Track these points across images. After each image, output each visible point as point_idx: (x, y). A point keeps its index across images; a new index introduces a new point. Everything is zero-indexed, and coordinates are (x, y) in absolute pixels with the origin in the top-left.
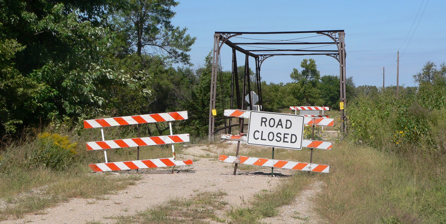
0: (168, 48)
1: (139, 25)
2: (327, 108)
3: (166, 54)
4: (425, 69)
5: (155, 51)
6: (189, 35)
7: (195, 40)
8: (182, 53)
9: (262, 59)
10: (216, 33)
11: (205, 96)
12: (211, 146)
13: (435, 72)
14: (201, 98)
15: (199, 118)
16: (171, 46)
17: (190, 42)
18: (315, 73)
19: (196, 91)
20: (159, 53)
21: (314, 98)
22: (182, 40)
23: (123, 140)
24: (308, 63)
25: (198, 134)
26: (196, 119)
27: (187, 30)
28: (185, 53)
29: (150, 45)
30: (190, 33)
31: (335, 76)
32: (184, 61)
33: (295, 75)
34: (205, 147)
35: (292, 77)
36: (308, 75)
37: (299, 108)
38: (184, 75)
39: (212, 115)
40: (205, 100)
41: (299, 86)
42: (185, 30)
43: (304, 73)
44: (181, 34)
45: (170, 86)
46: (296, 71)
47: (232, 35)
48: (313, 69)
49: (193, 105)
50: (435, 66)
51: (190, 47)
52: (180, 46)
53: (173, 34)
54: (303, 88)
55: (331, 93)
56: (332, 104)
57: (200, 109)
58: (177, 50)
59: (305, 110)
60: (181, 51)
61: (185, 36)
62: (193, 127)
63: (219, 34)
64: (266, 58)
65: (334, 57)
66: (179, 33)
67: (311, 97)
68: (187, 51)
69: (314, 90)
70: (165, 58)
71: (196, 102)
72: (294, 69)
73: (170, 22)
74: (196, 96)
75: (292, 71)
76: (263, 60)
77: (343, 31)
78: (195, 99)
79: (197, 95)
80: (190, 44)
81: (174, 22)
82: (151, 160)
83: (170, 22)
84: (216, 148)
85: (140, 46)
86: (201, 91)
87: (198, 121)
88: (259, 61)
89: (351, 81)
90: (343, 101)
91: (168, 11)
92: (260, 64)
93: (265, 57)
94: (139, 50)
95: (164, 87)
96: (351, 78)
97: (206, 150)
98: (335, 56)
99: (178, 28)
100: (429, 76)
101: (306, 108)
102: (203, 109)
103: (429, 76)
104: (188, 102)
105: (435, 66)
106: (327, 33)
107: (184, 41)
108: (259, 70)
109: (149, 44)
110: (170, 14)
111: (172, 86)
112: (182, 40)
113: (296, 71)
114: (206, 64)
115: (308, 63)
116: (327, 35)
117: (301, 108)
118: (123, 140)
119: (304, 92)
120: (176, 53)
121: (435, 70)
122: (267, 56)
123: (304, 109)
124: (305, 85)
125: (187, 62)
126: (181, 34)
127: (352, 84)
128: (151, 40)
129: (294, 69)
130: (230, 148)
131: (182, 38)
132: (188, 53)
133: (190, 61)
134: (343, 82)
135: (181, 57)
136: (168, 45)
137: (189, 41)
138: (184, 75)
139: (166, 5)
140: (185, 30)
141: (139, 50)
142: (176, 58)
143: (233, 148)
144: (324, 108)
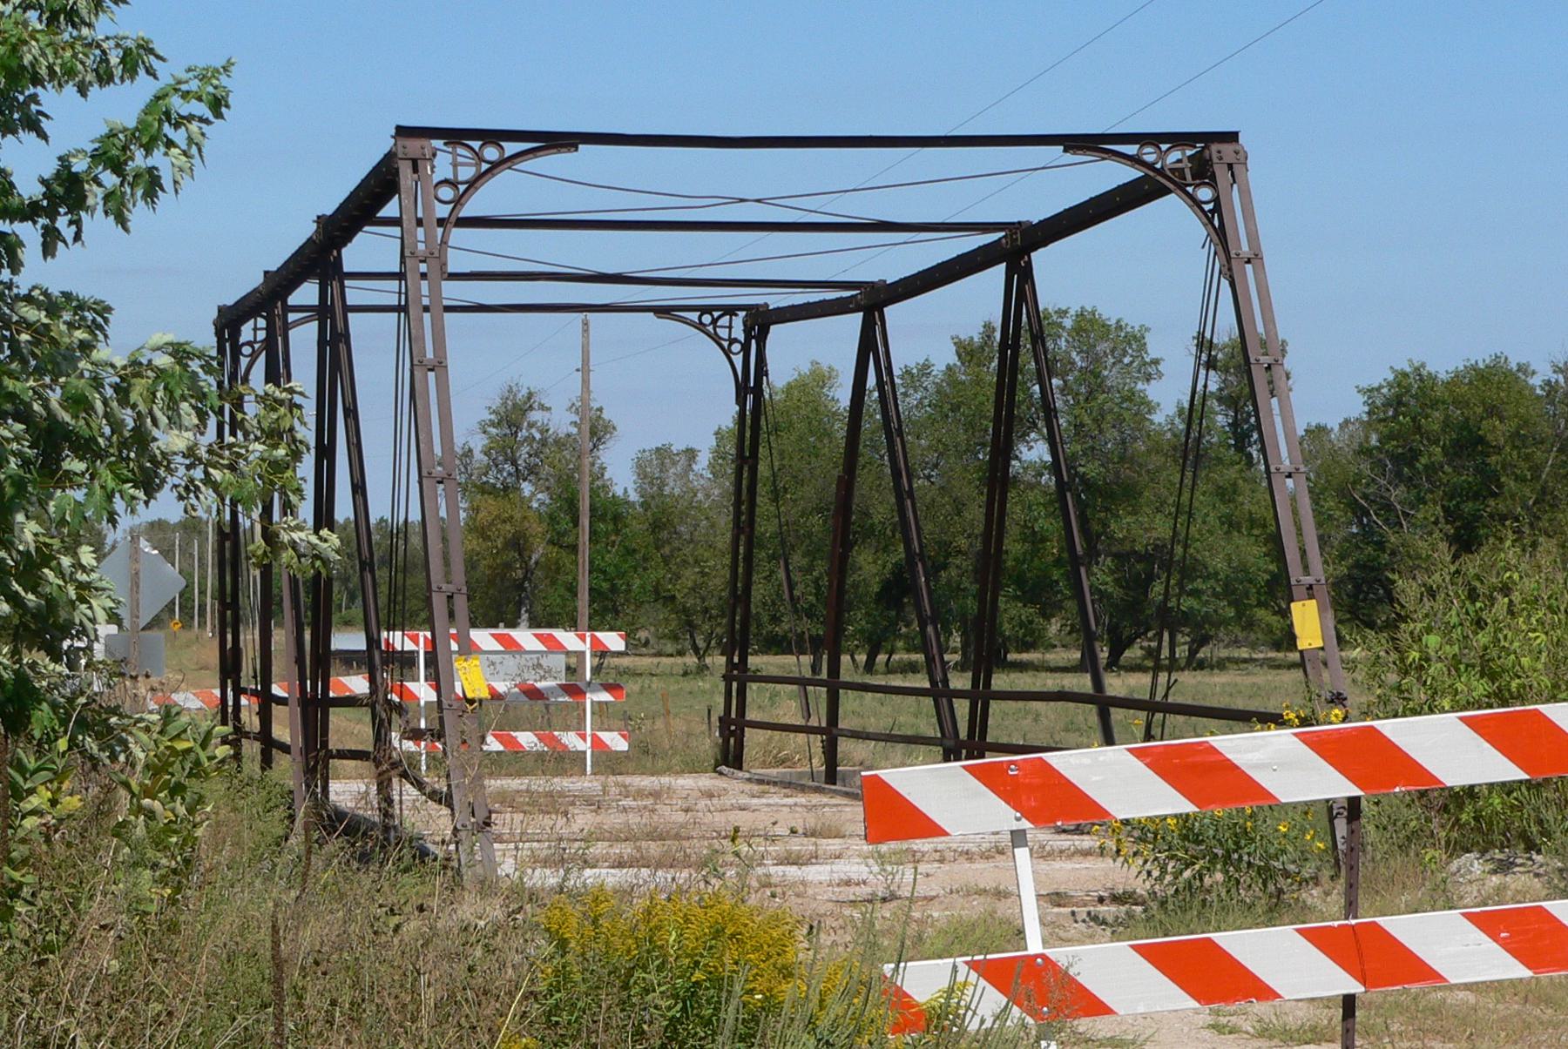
2: (613, 641)
4: (492, 424)
10: (402, 132)
13: (543, 442)
23: (1188, 807)
47: (511, 148)
50: (542, 407)
59: (479, 651)
65: (700, 326)
77: (1232, 137)
82: (1380, 920)
90: (1310, 592)
98: (707, 319)
100: (514, 463)
103: (514, 463)
105: (542, 407)
106: (1131, 149)
118: (1188, 807)
121: (544, 431)
144: (596, 642)
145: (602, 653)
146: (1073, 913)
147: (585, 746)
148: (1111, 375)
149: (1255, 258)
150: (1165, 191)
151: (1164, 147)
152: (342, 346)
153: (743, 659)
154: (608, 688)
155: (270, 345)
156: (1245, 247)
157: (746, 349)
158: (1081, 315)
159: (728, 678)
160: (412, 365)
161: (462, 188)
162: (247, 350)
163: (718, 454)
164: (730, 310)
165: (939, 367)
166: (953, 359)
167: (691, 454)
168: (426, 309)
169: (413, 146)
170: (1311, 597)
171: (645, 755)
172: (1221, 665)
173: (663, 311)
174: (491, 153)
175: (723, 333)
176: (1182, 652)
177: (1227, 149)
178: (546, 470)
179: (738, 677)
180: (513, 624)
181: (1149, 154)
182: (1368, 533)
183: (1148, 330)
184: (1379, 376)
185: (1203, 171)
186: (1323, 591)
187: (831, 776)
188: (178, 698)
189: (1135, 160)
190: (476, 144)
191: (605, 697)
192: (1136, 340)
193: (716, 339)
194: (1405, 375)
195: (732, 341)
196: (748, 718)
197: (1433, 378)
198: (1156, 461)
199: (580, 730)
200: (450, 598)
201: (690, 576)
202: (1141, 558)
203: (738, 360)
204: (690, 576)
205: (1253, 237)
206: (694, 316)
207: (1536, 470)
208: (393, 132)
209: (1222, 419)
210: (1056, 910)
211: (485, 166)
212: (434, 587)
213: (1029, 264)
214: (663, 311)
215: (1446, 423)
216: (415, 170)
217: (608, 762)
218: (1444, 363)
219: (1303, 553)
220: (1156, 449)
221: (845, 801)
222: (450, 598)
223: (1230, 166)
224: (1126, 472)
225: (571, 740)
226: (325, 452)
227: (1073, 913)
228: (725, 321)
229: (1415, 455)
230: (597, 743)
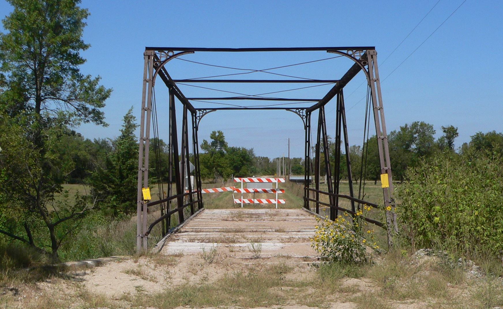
0: (76, 103)
1: (38, 74)
3: (72, 109)
5: (59, 107)
6: (102, 86)
7: (111, 93)
8: (94, 110)
9: (201, 115)
10: (147, 49)
11: (124, 164)
12: (142, 261)
14: (118, 167)
15: (116, 193)
16: (80, 99)
17: (104, 95)
18: (223, 144)
19: (111, 159)
20: (64, 109)
21: (222, 167)
22: (94, 92)
24: (217, 134)
25: (115, 214)
26: (112, 195)
27: (100, 80)
28: (98, 109)
29: (53, 98)
30: (104, 83)
31: (238, 147)
32: (96, 120)
34: (130, 264)
36: (216, 146)
37: (246, 180)
38: (100, 146)
39: (143, 199)
40: (124, 169)
41: (209, 155)
42: (97, 79)
43: (213, 144)
44: (92, 85)
45: (87, 157)
47: (176, 52)
48: (221, 140)
49: (108, 176)
51: (104, 102)
52: (92, 102)
53: (82, 85)
55: (234, 162)
56: (236, 172)
57: (117, 181)
58: (88, 105)
59: (254, 182)
60: (93, 107)
61: (97, 87)
62: (109, 205)
63: (152, 51)
64: (206, 113)
65: (296, 112)
66: (90, 83)
67: (219, 166)
68: (99, 107)
69: (223, 160)
70: (71, 115)
71: (113, 172)
72: (204, 140)
73: (78, 70)
74: (112, 165)
76: (202, 116)
77: (373, 48)
78: (112, 169)
79: (114, 163)
80: (104, 98)
81: (83, 70)
83: (78, 70)
84: (152, 266)
85: (39, 100)
86: (119, 158)
87: (114, 197)
88: (196, 118)
89: (252, 152)
90: (386, 172)
91: (76, 56)
92: (198, 121)
93: (205, 111)
94: (38, 105)
95: (81, 157)
96: (252, 149)
97: (133, 272)
98: (297, 111)
99: (88, 77)
101: (255, 179)
102: (121, 182)
104: (101, 172)
106: (345, 51)
107: (96, 93)
108: (197, 130)
109: (50, 98)
110: (77, 60)
111: (89, 157)
112: (94, 92)
114: (124, 125)
115: (217, 134)
116: (347, 55)
117: (258, 179)
119: (214, 162)
120: (86, 109)
122: (207, 111)
123: (252, 181)
125: (101, 121)
126: (92, 85)
127: (253, 155)
128: (54, 95)
129: (204, 140)
130: (180, 265)
131: (93, 91)
132: (101, 110)
133: (104, 120)
135: (92, 115)
136: (76, 98)
137: (103, 93)
138: (100, 146)
139: (73, 48)
140: (97, 79)
141: (38, 105)
142: (86, 116)
143: (185, 264)
147: (276, 202)
148: (427, 133)
149: (377, 80)
151: (354, 51)
154: (281, 190)
156: (375, 77)
157: (306, 117)
158: (421, 123)
162: (198, 118)
164: (303, 109)
165: (397, 131)
166: (400, 130)
167: (359, 147)
173: (288, 109)
174: (171, 54)
175: (301, 114)
177: (371, 51)
180: (252, 176)
183: (87, 25)
184: (474, 134)
186: (390, 171)
190: (166, 52)
191: (281, 192)
192: (431, 127)
193: (300, 115)
194: (478, 134)
195: (303, 116)
196: (339, 194)
197: (483, 134)
198: (434, 148)
203: (305, 120)
205: (377, 75)
206: (295, 110)
209: (446, 141)
210: (304, 262)
214: (288, 109)
215: (485, 142)
217: (281, 206)
218: (485, 132)
219: (385, 160)
220: (435, 146)
222: (143, 172)
223: (372, 56)
224: (429, 150)
225: (273, 201)
228: (301, 111)
230: (279, 202)
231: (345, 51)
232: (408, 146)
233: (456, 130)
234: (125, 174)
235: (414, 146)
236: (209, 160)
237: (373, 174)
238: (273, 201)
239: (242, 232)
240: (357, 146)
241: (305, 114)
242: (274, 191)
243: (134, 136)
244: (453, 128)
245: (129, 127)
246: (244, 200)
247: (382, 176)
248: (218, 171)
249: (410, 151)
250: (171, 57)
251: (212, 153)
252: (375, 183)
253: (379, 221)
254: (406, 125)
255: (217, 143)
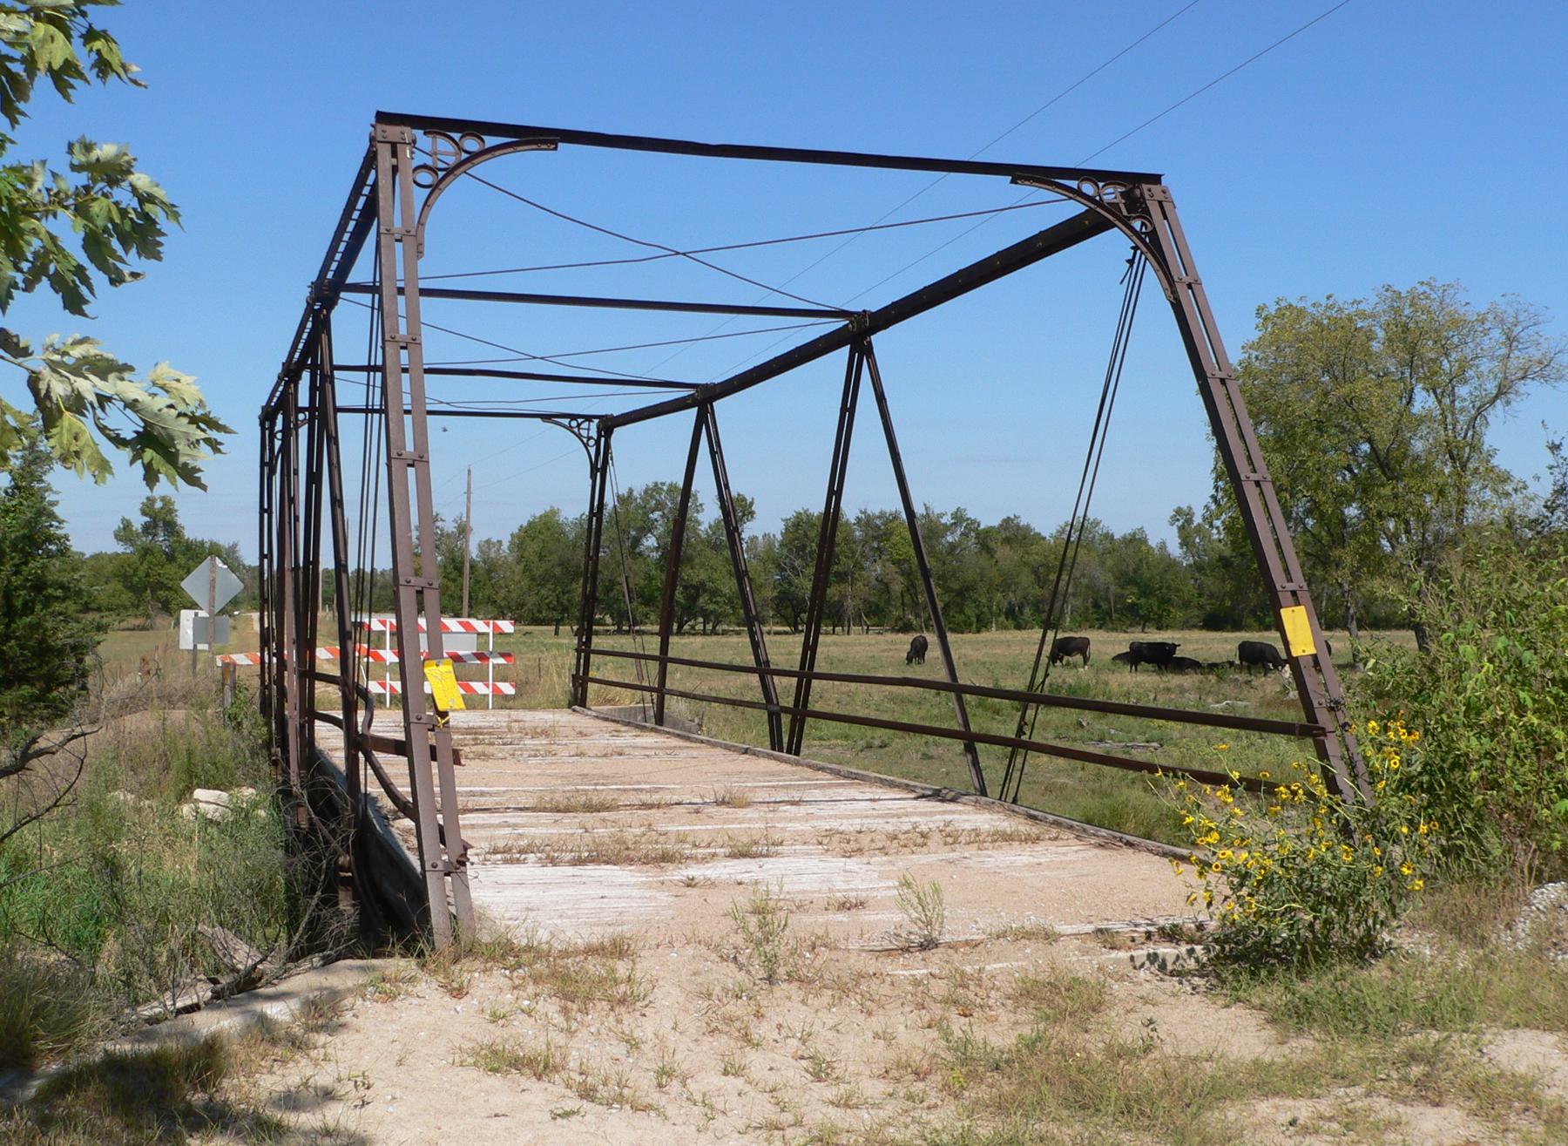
2: (507, 626)
10: (383, 118)
18: (171, 528)
24: (158, 505)
33: (124, 533)
35: (118, 537)
36: (155, 535)
41: (136, 558)
43: (147, 529)
46: (127, 525)
47: (491, 141)
54: (145, 566)
63: (407, 129)
65: (570, 428)
72: (123, 520)
75: (117, 524)
77: (1155, 179)
96: (235, 545)
98: (574, 423)
106: (1073, 184)
113: (127, 525)
115: (158, 505)
119: (148, 575)
124: (149, 558)
129: (123, 520)
134: (1254, 477)
144: (496, 626)
145: (499, 633)
146: (1132, 958)
147: (489, 691)
150: (1104, 226)
152: (328, 386)
153: (589, 640)
154: (503, 655)
155: (398, 633)
157: (598, 443)
159: (579, 651)
160: (384, 341)
161: (441, 174)
163: (512, 543)
164: (589, 418)
168: (401, 291)
169: (394, 132)
170: (1298, 604)
171: (523, 697)
172: (724, 633)
173: (547, 417)
174: (472, 144)
175: (584, 433)
176: (709, 627)
178: (443, 547)
179: (585, 651)
181: (1088, 188)
182: (784, 578)
184: (790, 514)
185: (1136, 206)
187: (660, 719)
188: (234, 657)
189: (1078, 194)
190: (456, 136)
191: (502, 661)
193: (579, 436)
195: (589, 438)
199: (484, 680)
200: (420, 593)
201: (502, 593)
202: (693, 587)
203: (593, 450)
204: (502, 593)
206: (566, 421)
207: (853, 553)
208: (373, 121)
211: (464, 156)
212: (402, 581)
213: (870, 343)
214: (547, 417)
216: (394, 154)
220: (702, 541)
221: (681, 743)
222: (420, 593)
225: (479, 687)
226: (314, 478)
227: (1132, 958)
228: (585, 425)
229: (804, 547)
231: (1073, 184)
232: (637, 542)
233: (752, 504)
234: (18, 603)
235: (650, 541)
236: (135, 571)
237: (554, 609)
238: (479, 687)
239: (608, 809)
240: (494, 540)
241: (594, 434)
242: (481, 656)
243: (48, 489)
244: (744, 499)
245: (33, 462)
246: (500, 685)
247: (1286, 614)
248: (158, 600)
249: (640, 554)
250: (473, 157)
251: (146, 552)
252: (557, 633)
253: (1106, 769)
254: (631, 491)
255: (156, 526)
